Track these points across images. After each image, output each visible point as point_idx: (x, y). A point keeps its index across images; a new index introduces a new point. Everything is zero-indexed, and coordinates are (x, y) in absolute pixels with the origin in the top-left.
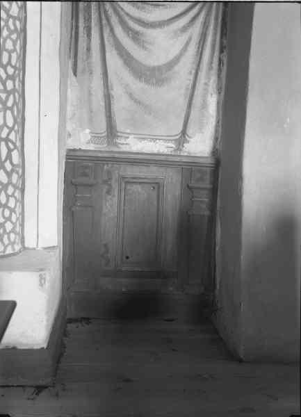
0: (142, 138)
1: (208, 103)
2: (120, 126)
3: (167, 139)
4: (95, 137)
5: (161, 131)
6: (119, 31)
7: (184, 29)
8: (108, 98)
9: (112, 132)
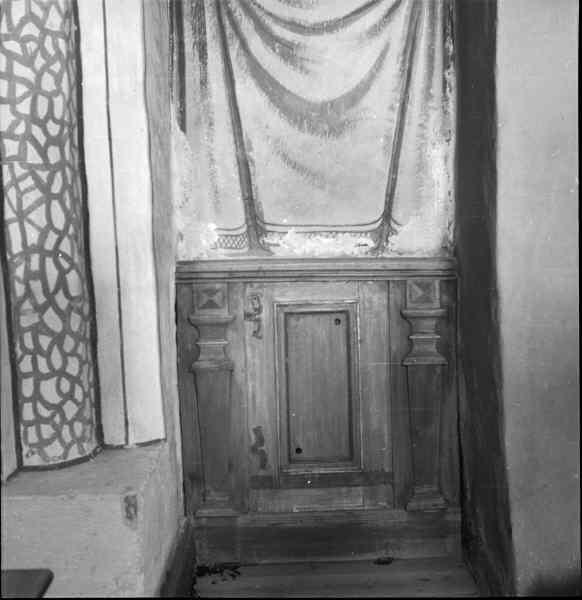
2: (269, 214)
4: (228, 236)
5: (344, 216)
6: (256, 44)
7: (375, 31)
8: (245, 166)
9: (256, 225)
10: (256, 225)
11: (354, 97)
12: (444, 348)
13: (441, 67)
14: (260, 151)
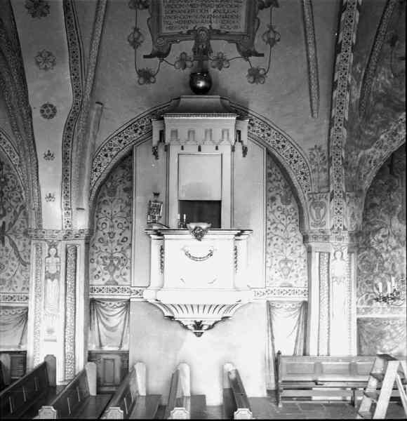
0: (109, 346)
1: (220, 413)
2: (103, 344)
3: (117, 346)
4: (96, 347)
5: (115, 344)
6: (102, 318)
7: (120, 316)
8: (100, 336)
9: (101, 345)
10: (101, 345)
11: (117, 326)
12: (209, 223)
13: (166, 133)
14: (102, 334)
